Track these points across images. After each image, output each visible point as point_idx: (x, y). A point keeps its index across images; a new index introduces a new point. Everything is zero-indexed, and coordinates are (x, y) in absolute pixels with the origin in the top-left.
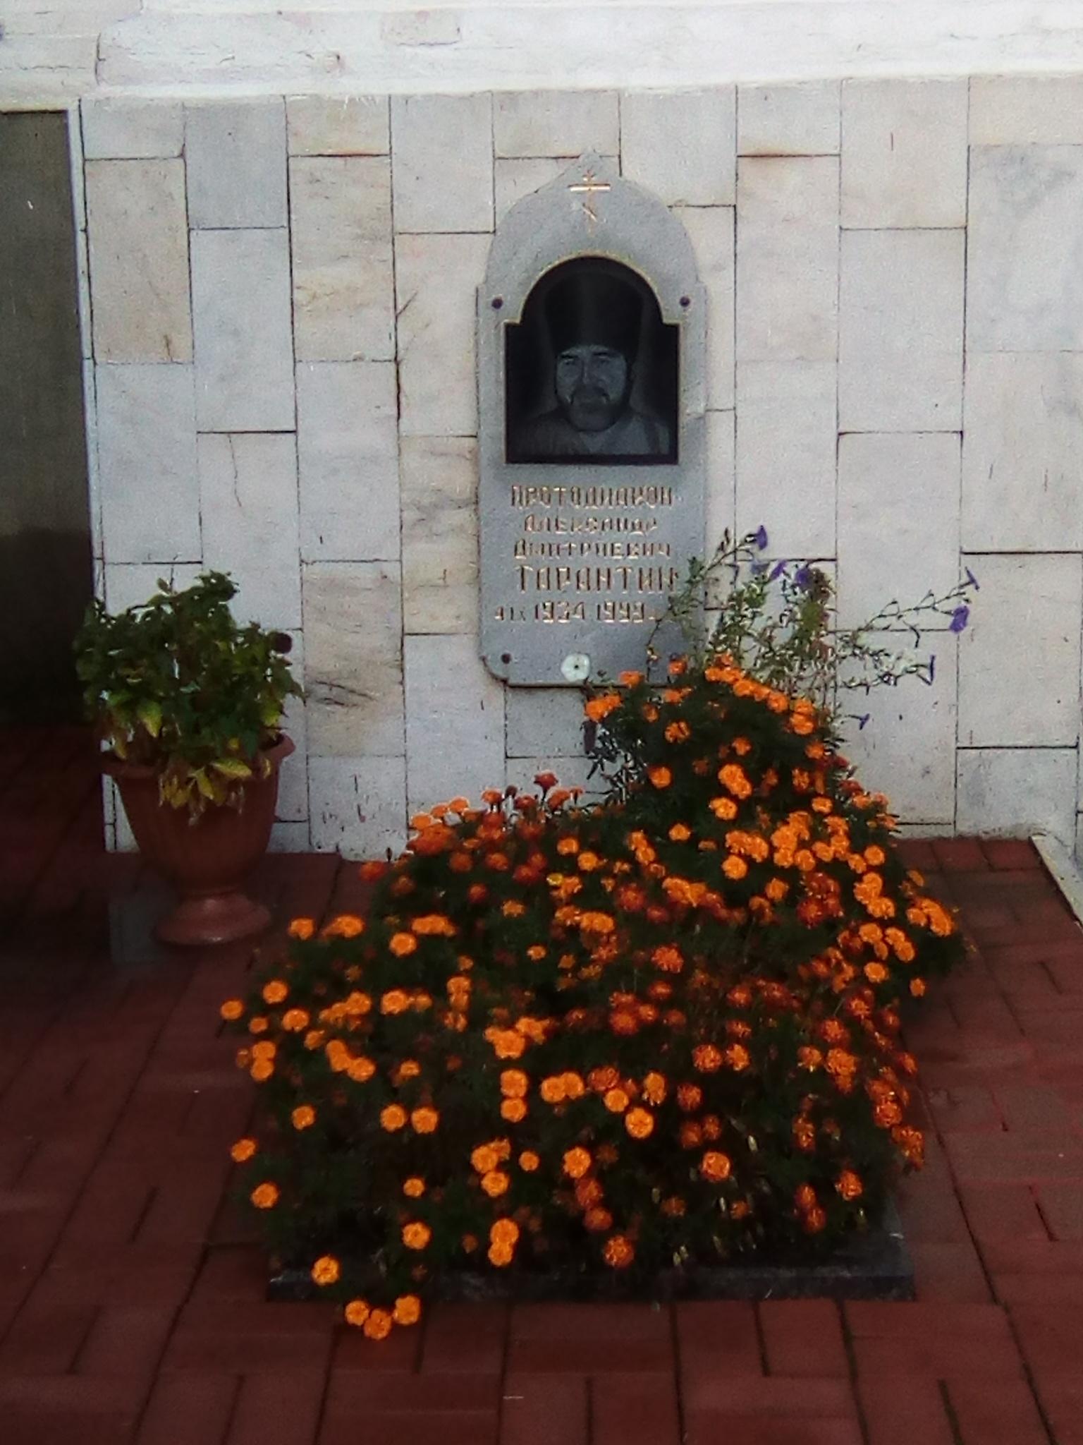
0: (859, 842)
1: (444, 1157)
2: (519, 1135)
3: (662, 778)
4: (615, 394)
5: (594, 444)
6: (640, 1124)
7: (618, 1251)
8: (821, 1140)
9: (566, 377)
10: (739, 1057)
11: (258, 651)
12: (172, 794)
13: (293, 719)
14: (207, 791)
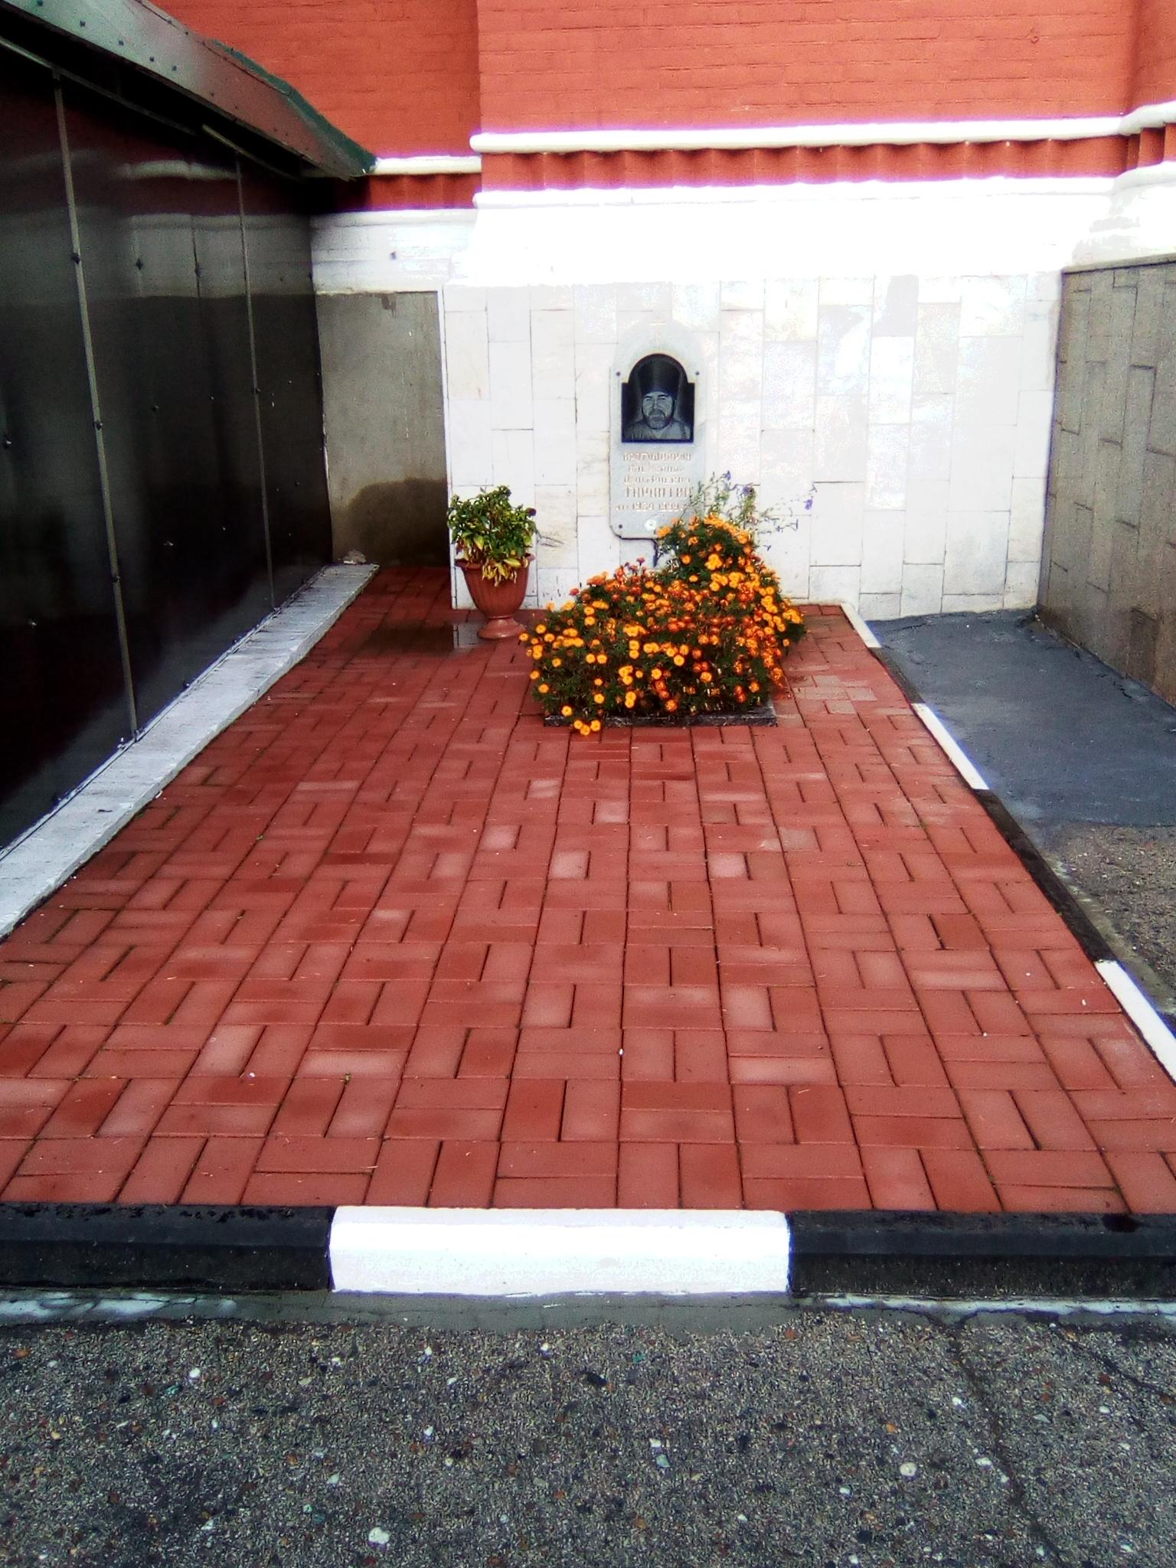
0: (764, 584)
1: (608, 672)
2: (637, 664)
3: (686, 560)
4: (668, 413)
5: (658, 435)
6: (679, 661)
7: (671, 705)
8: (745, 670)
9: (647, 406)
10: (715, 640)
11: (522, 516)
12: (488, 573)
13: (533, 543)
14: (502, 572)
